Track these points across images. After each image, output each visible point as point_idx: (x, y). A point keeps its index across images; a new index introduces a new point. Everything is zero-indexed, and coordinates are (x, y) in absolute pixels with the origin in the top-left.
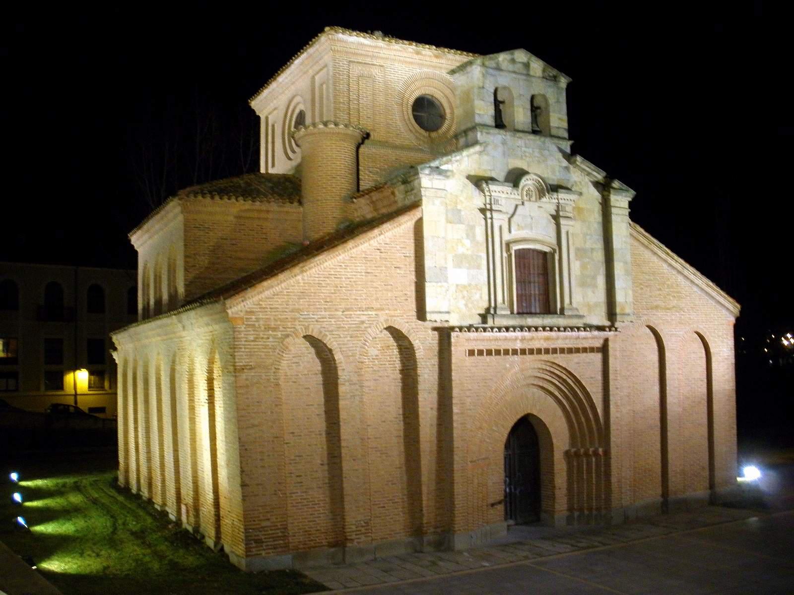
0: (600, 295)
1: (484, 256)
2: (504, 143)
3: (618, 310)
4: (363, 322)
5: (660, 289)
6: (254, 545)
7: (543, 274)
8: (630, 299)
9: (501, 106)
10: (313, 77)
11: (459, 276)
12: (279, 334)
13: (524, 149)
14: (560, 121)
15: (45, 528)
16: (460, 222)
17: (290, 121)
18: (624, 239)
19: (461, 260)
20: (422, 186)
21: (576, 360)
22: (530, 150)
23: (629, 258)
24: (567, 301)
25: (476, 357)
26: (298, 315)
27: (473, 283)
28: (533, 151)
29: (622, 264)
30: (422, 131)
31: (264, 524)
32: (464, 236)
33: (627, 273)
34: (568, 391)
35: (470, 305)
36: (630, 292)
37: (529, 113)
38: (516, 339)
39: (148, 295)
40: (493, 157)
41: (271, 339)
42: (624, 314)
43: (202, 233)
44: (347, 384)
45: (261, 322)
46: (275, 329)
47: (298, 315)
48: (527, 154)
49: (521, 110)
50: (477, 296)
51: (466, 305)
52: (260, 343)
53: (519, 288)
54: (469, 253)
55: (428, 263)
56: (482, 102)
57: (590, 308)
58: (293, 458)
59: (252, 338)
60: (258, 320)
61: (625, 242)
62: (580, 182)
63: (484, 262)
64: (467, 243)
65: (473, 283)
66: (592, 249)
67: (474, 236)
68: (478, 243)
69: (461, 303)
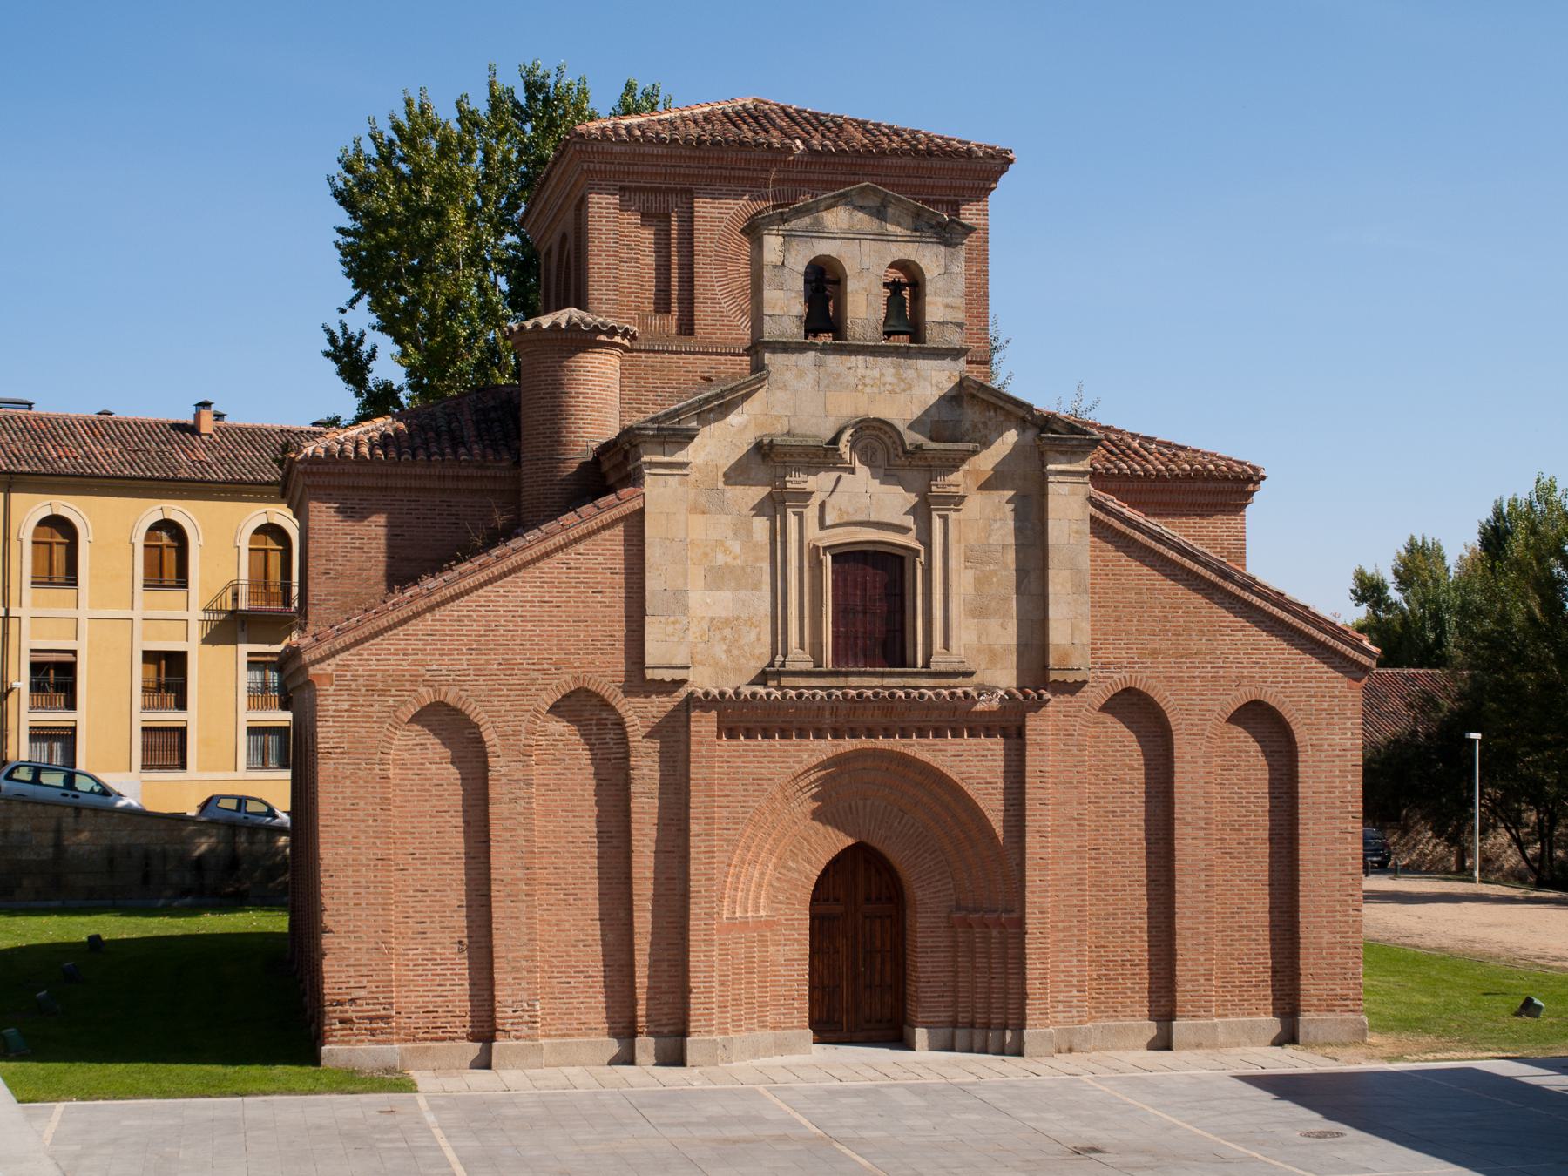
0: (1006, 634)
1: (766, 566)
3: (1052, 661)
6: (338, 1026)
7: (233, 863)
8: (1085, 638)
11: (706, 603)
14: (948, 310)
15: (977, 472)
18: (1075, 527)
19: (717, 578)
21: (952, 750)
22: (876, 373)
23: (1085, 561)
27: (744, 616)
29: (1067, 573)
32: (730, 534)
35: (735, 652)
36: (1086, 626)
41: (376, 707)
47: (422, 670)
48: (867, 381)
50: (753, 636)
51: (728, 652)
52: (816, 177)
54: (739, 562)
55: (653, 583)
57: (993, 657)
59: (345, 706)
61: (1077, 532)
62: (984, 423)
63: (767, 578)
64: (736, 547)
65: (744, 616)
68: (756, 545)
69: (719, 651)
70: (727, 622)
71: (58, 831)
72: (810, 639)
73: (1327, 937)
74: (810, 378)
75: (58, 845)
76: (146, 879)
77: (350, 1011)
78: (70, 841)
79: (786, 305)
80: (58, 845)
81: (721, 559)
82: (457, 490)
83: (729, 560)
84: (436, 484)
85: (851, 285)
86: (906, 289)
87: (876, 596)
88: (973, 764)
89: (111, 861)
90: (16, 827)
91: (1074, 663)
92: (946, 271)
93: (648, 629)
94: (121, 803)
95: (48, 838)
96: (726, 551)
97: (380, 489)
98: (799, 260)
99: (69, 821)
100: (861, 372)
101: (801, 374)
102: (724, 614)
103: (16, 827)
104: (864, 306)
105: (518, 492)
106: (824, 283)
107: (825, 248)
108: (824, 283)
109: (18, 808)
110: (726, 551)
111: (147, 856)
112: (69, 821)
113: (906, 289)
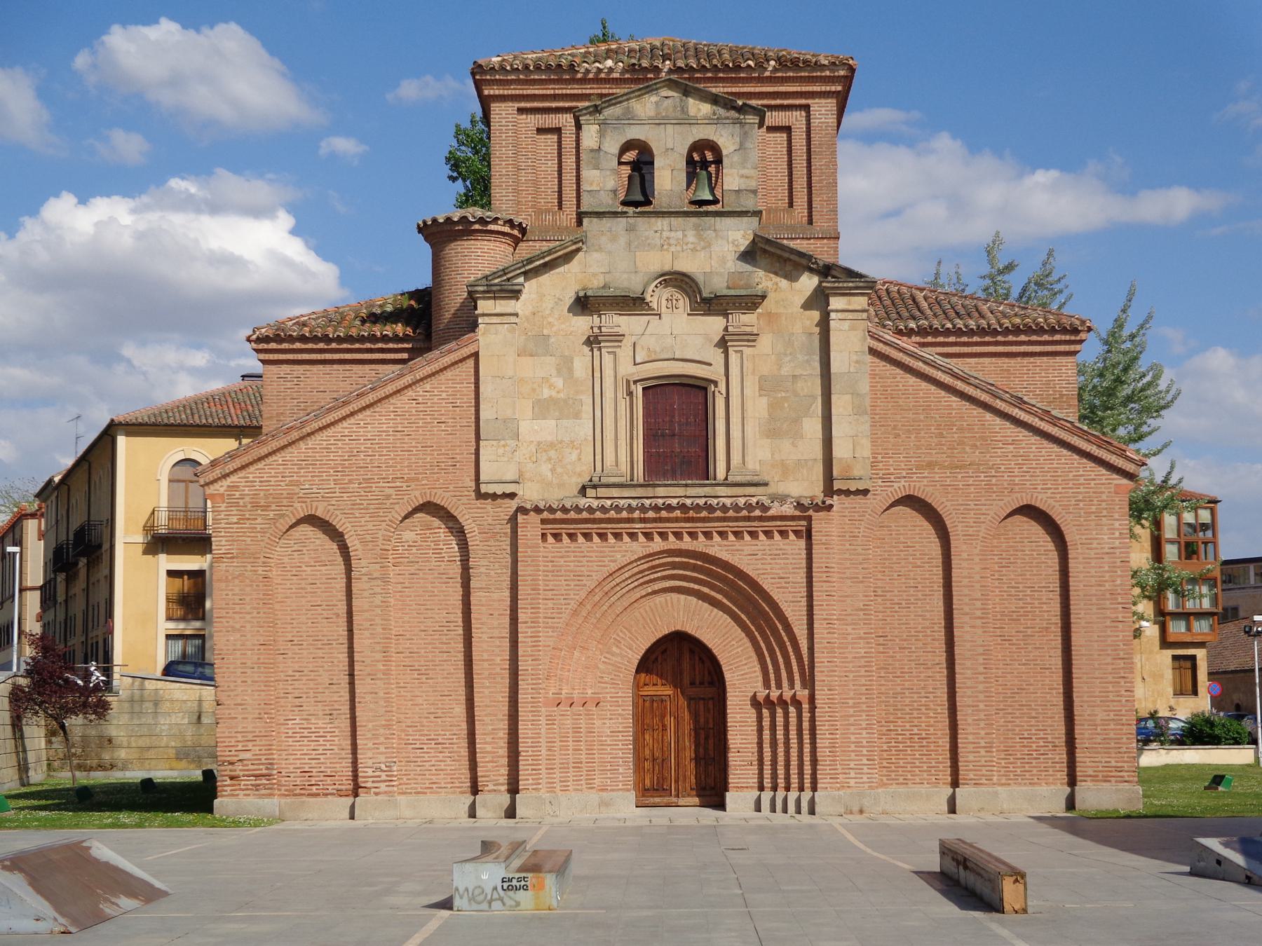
4: (388, 497)
8: (865, 451)
12: (271, 514)
16: (548, 353)
18: (854, 358)
22: (680, 234)
24: (736, 458)
25: (227, 639)
26: (297, 490)
27: (566, 439)
28: (685, 236)
31: (242, 756)
32: (554, 372)
33: (858, 411)
34: (726, 596)
35: (559, 470)
40: (610, 253)
44: (365, 578)
45: (247, 499)
46: (266, 508)
47: (297, 490)
49: (667, 173)
50: (574, 457)
51: (553, 470)
53: (102, 596)
54: (562, 395)
56: (597, 172)
57: (786, 470)
58: (290, 673)
64: (559, 383)
65: (566, 439)
67: (571, 370)
72: (624, 452)
73: (1101, 715)
74: (622, 241)
77: (238, 769)
79: (604, 181)
83: (554, 394)
86: (703, 161)
87: (679, 419)
88: (770, 562)
91: (856, 472)
92: (741, 147)
96: (551, 386)
98: (612, 146)
100: (665, 234)
101: (614, 239)
102: (549, 438)
104: (668, 178)
106: (640, 163)
108: (640, 163)
110: (551, 386)
113: (703, 161)
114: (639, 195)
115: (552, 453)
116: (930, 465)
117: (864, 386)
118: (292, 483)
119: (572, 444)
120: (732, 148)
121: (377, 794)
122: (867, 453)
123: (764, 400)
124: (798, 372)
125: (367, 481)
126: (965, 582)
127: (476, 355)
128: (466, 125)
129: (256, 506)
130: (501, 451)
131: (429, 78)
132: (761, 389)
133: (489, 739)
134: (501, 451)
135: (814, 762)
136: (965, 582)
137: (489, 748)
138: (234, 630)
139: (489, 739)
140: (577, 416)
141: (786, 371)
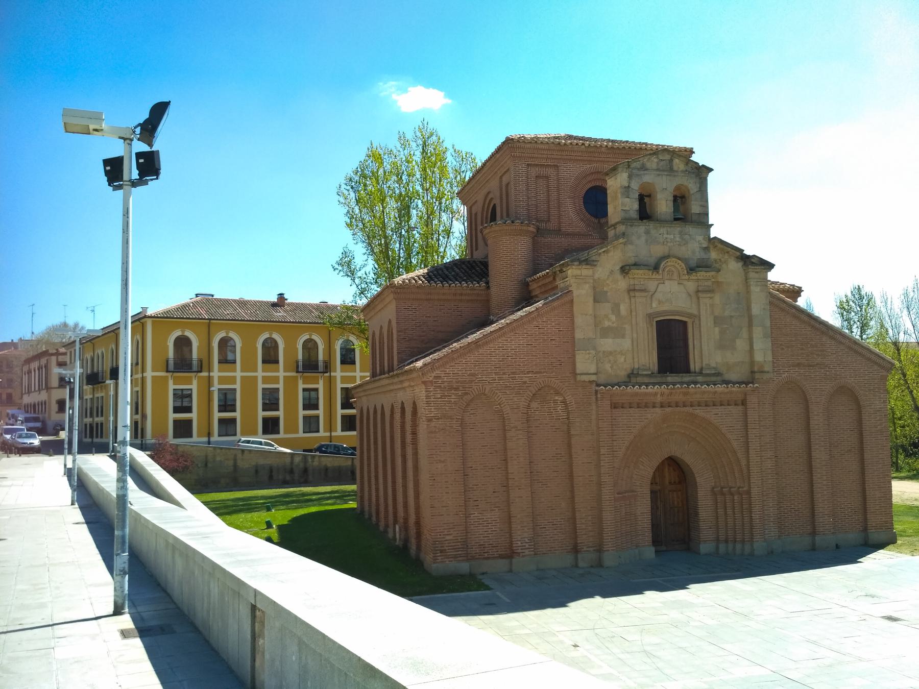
2: (647, 232)
4: (525, 383)
5: (802, 349)
9: (646, 200)
10: (501, 177)
12: (460, 393)
13: (665, 236)
17: (487, 212)
20: (85, 525)
22: (672, 236)
30: (593, 219)
36: (770, 353)
37: (671, 204)
38: (656, 394)
39: (393, 353)
42: (762, 372)
43: (410, 313)
49: (664, 202)
50: (622, 360)
60: (443, 382)
64: (613, 318)
66: (731, 317)
67: (619, 310)
70: (611, 353)
71: (235, 460)
72: (649, 358)
74: (643, 239)
75: (235, 466)
76: (271, 477)
78: (240, 464)
80: (235, 466)
81: (607, 324)
82: (461, 300)
83: (610, 324)
84: (95, 405)
85: (659, 196)
88: (725, 419)
89: (257, 471)
90: (218, 459)
91: (766, 369)
93: (577, 356)
94: (149, 453)
95: (231, 463)
96: (609, 320)
97: (427, 300)
99: (239, 456)
100: (665, 236)
101: (639, 237)
102: (609, 349)
103: (218, 459)
104: (663, 206)
105: (488, 301)
107: (648, 178)
109: (218, 451)
110: (609, 320)
111: (271, 470)
112: (239, 456)
114: (645, 213)
115: (611, 358)
116: (799, 365)
117: (768, 323)
118: (470, 375)
119: (621, 353)
120: (696, 190)
121: (523, 556)
122: (770, 358)
123: (717, 329)
124: (733, 314)
125: (513, 373)
126: (816, 427)
127: (572, 301)
128: (80, 325)
129: (451, 388)
130: (587, 356)
131: (28, 337)
132: (715, 323)
133: (583, 521)
134: (587, 356)
135: (416, 468)
136: (816, 427)
137: (584, 526)
138: (441, 461)
139: (583, 521)
140: (623, 337)
141: (727, 313)
